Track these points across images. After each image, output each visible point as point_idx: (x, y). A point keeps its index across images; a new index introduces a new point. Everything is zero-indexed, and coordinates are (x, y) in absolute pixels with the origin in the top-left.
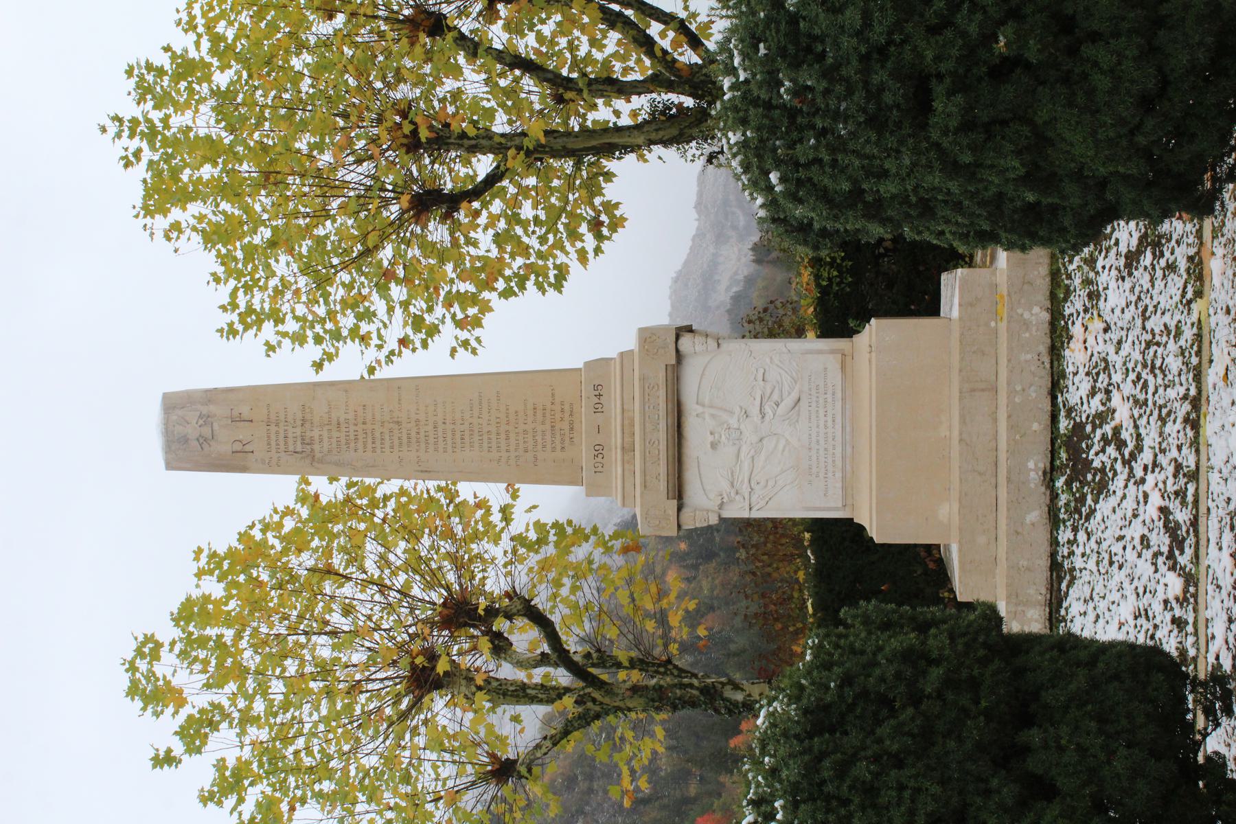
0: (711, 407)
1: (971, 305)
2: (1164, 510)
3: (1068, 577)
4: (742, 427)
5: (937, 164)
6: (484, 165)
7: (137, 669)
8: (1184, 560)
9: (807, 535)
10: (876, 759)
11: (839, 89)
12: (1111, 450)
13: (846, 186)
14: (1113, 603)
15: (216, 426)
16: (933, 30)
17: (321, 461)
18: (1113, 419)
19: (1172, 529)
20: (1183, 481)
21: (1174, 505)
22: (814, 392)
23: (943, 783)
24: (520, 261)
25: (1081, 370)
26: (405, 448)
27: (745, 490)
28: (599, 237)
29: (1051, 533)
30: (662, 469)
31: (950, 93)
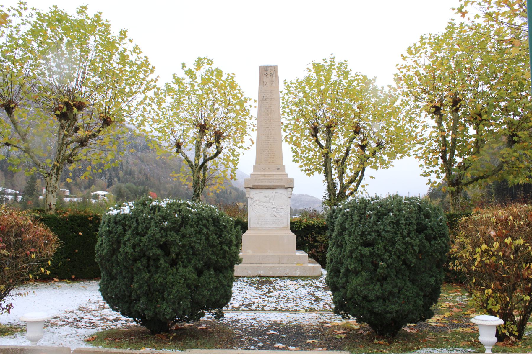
2: (254, 303)
5: (352, 248)
6: (323, 143)
8: (243, 307)
10: (207, 234)
11: (371, 225)
12: (267, 291)
13: (347, 227)
16: (384, 247)
19: (250, 305)
20: (262, 307)
21: (255, 305)
23: (202, 250)
27: (254, 204)
28: (306, 170)
31: (370, 251)
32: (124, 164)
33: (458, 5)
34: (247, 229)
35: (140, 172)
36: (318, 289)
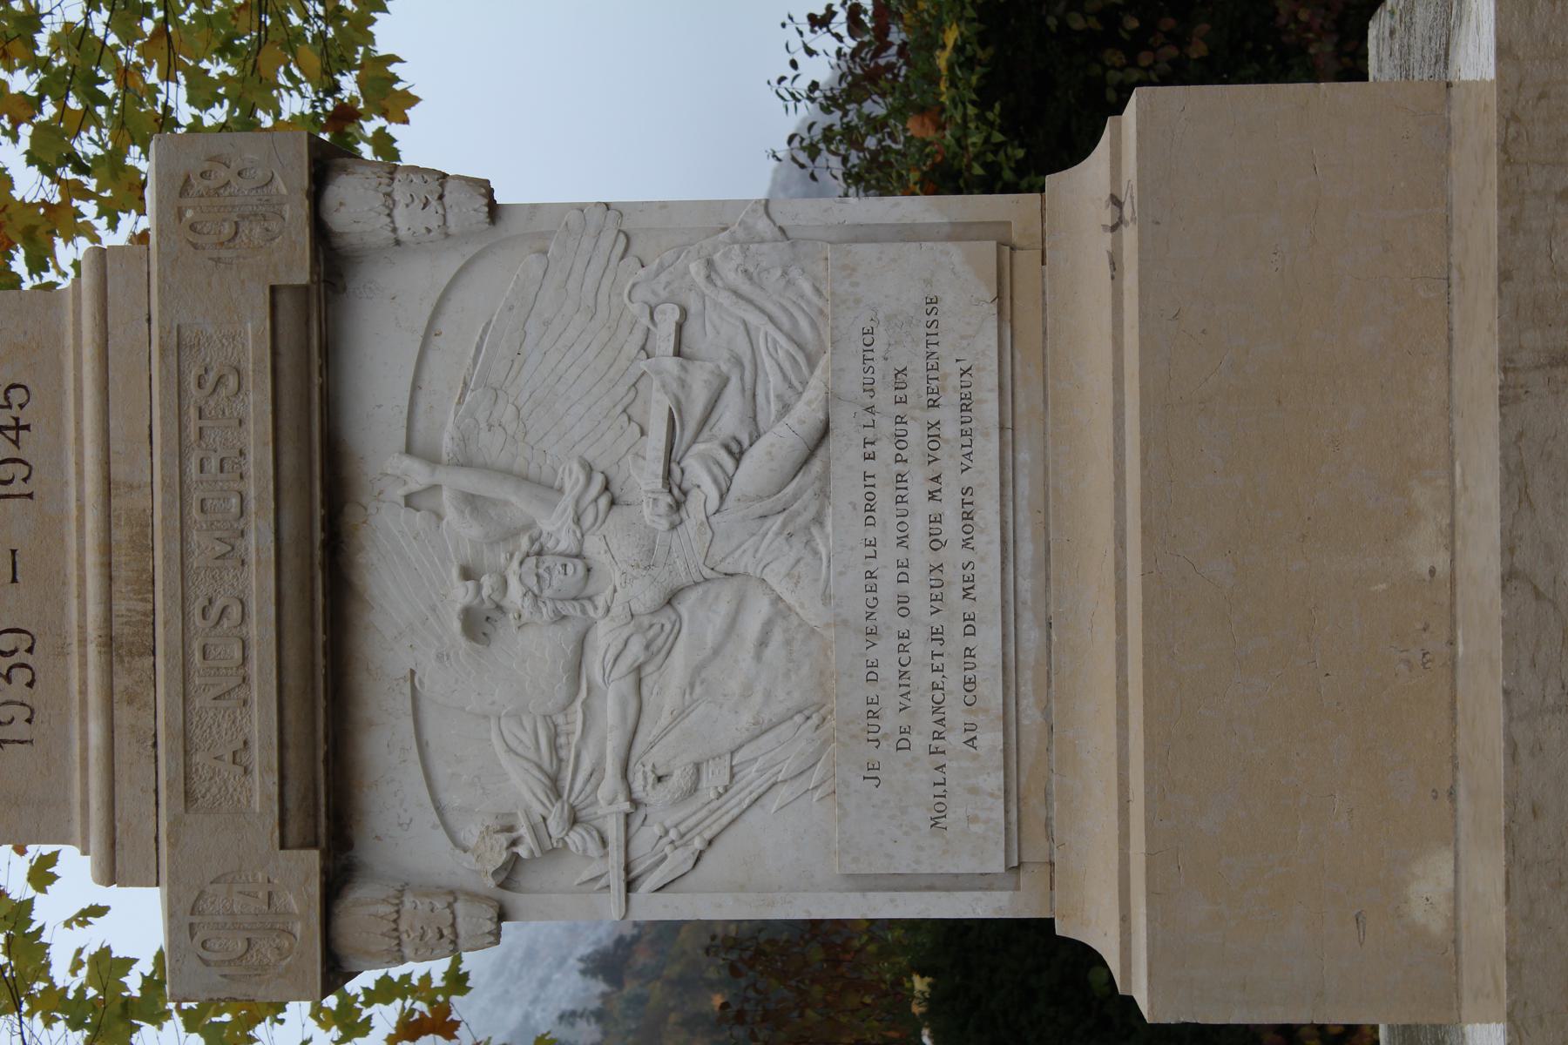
0: (465, 463)
4: (593, 546)
9: (920, 984)
22: (884, 396)
27: (608, 809)
30: (259, 723)
33: (6, 140)
34: (1036, 933)
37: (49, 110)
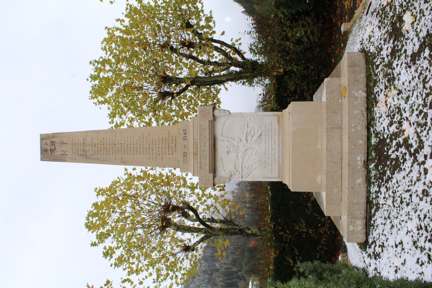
0: (227, 137)
1: (331, 93)
3: (375, 207)
4: (239, 145)
7: (89, 220)
9: (269, 187)
12: (403, 150)
14: (403, 221)
15: (56, 145)
17: (89, 158)
18: (403, 135)
22: (267, 131)
24: (195, 114)
25: (384, 115)
26: (117, 154)
29: (367, 188)
30: (207, 161)
32: (227, 266)
35: (234, 253)
36: (398, 51)
37: (188, 103)
